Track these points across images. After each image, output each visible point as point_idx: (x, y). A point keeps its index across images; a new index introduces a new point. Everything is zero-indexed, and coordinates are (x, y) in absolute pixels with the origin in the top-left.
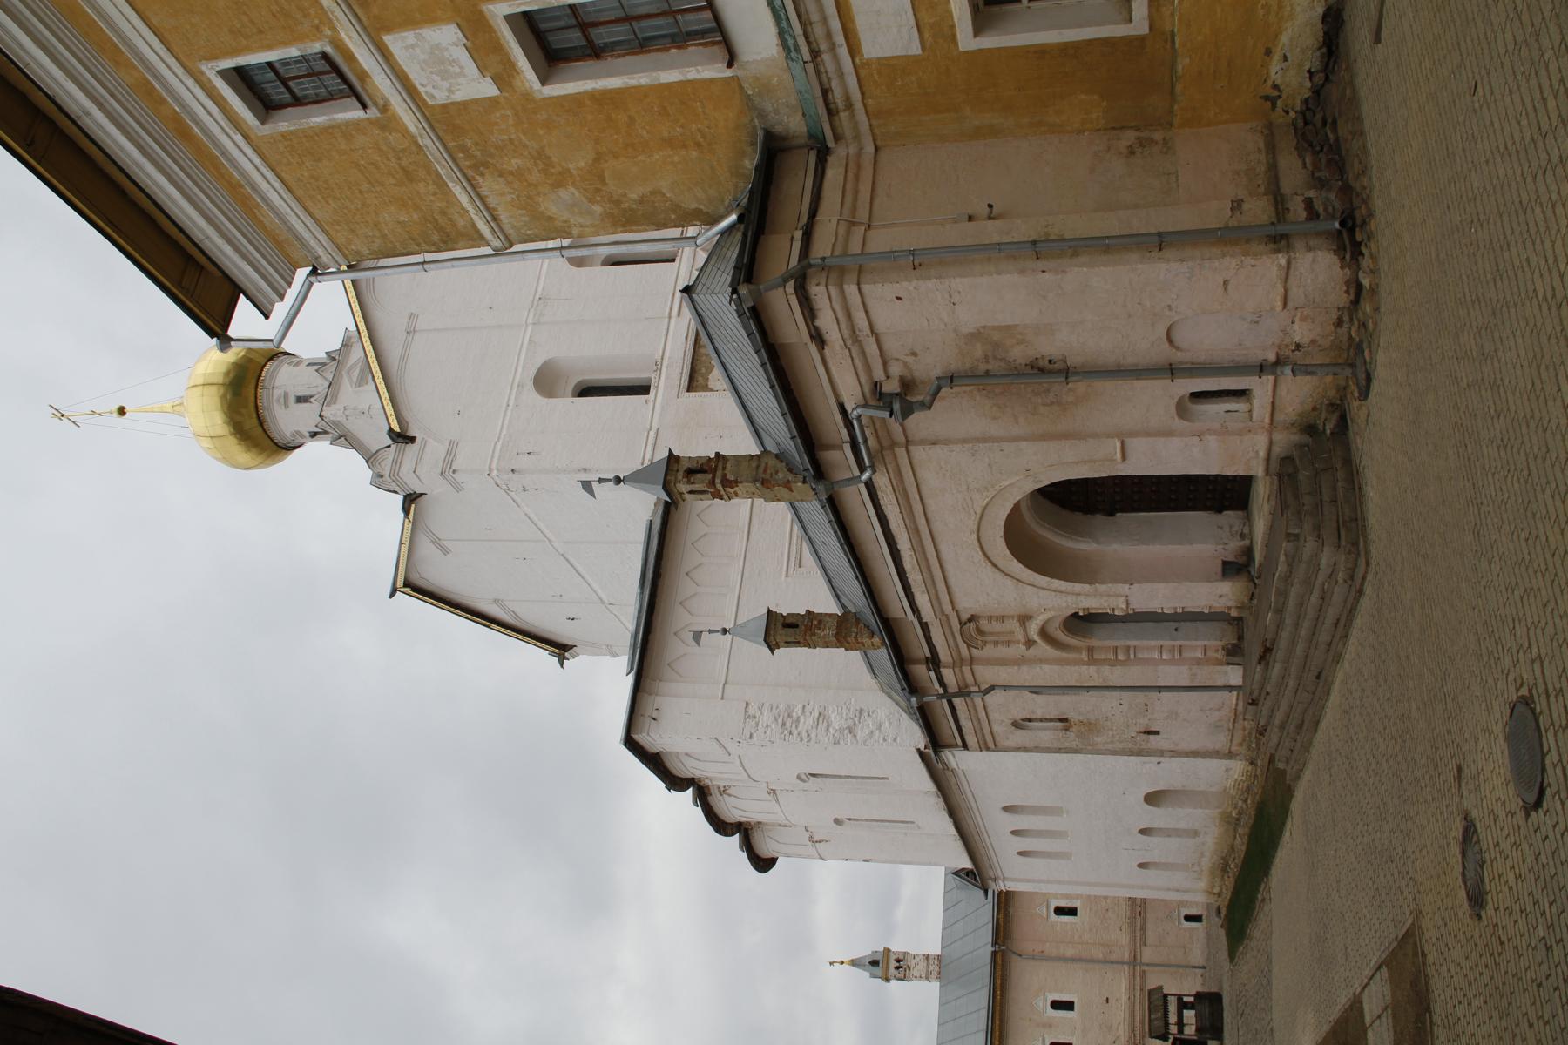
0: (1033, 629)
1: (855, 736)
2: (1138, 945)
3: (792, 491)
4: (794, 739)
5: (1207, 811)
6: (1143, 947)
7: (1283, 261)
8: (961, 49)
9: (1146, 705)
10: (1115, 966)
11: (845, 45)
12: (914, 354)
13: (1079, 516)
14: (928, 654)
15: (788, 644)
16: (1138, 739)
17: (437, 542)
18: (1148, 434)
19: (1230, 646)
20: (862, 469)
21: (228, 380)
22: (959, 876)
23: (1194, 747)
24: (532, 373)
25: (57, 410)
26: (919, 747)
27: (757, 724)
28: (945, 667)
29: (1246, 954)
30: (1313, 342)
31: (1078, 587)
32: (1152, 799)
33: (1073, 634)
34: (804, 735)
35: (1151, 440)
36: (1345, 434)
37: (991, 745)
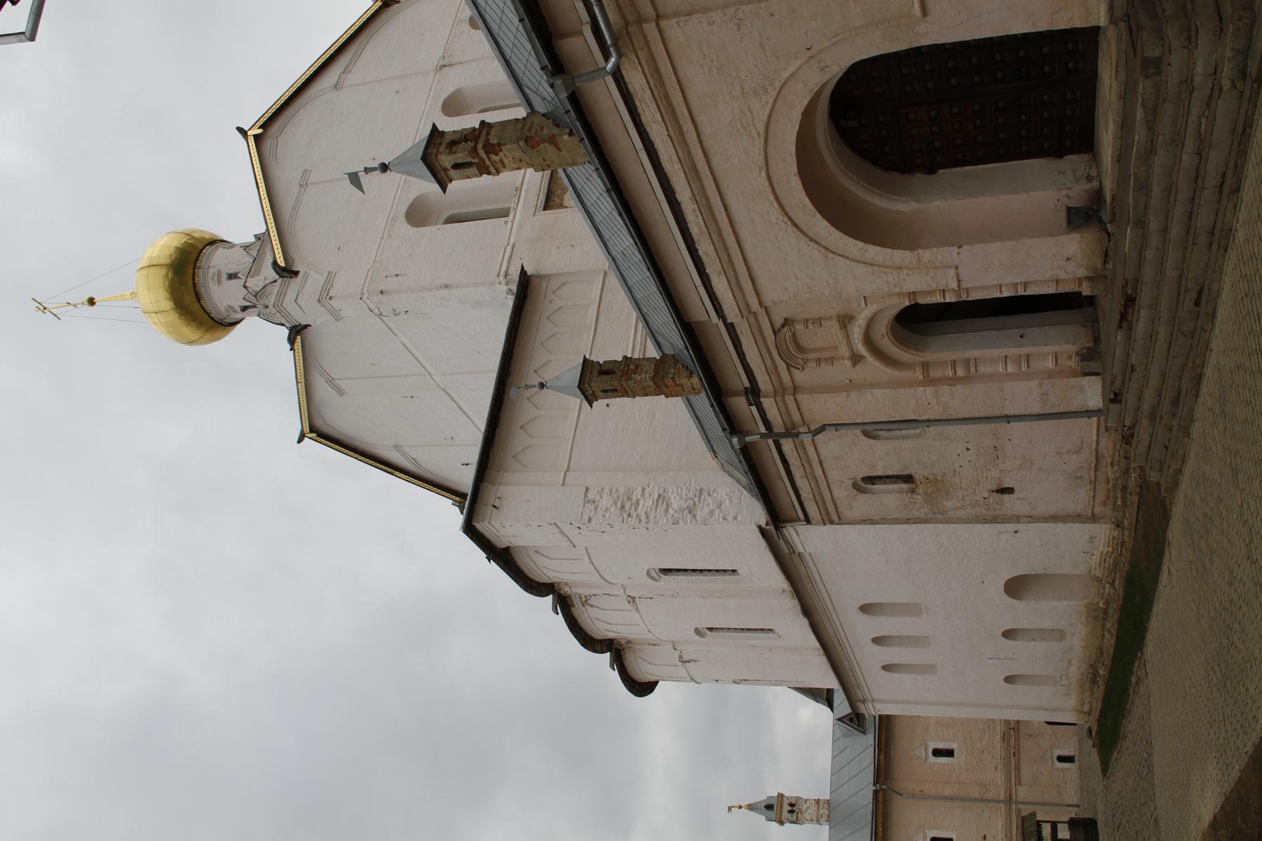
1: (695, 516)
2: (1013, 785)
3: (559, 149)
4: (633, 521)
6: (1018, 786)
10: (991, 804)
13: (895, 176)
14: (747, 384)
16: (991, 501)
17: (331, 381)
19: (1085, 351)
21: (168, 261)
23: (1053, 510)
24: (405, 207)
25: (40, 303)
26: (761, 524)
27: (596, 508)
28: (765, 397)
29: (1120, 758)
31: (898, 256)
32: (1016, 587)
34: (643, 517)
37: (836, 519)
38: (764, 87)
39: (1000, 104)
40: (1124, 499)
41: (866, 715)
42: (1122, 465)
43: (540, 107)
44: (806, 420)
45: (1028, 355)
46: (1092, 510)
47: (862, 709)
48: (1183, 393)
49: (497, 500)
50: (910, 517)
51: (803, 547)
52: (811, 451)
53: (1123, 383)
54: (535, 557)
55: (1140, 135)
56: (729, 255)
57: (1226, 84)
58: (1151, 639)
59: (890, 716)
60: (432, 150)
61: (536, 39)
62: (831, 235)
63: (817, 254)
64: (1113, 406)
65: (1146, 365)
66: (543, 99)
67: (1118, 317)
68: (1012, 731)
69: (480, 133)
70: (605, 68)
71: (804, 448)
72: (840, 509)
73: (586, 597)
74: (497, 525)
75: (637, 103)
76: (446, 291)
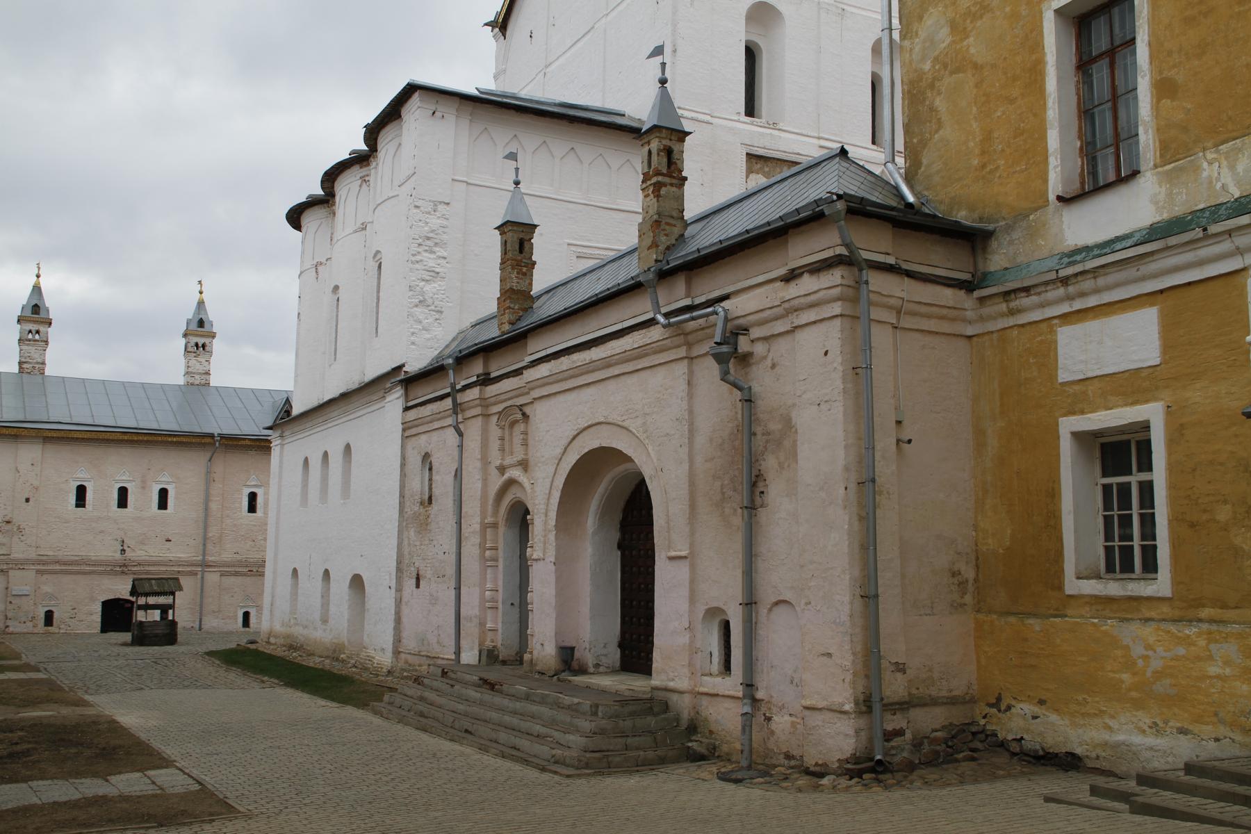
0: (515, 473)
1: (416, 306)
4: (414, 248)
5: (345, 631)
7: (847, 707)
8: (1060, 419)
9: (444, 576)
10: (201, 548)
11: (1071, 310)
12: (773, 366)
13: (618, 516)
14: (493, 375)
15: (505, 244)
16: (413, 569)
18: (692, 581)
20: (667, 315)
23: (404, 620)
27: (429, 213)
28: (481, 390)
30: (772, 733)
32: (357, 582)
34: (418, 258)
35: (687, 584)
44: (467, 421)
45: (497, 608)
49: (440, 114)
51: (389, 402)
54: (395, 143)
63: (559, 451)
67: (486, 678)
72: (414, 439)
73: (368, 181)
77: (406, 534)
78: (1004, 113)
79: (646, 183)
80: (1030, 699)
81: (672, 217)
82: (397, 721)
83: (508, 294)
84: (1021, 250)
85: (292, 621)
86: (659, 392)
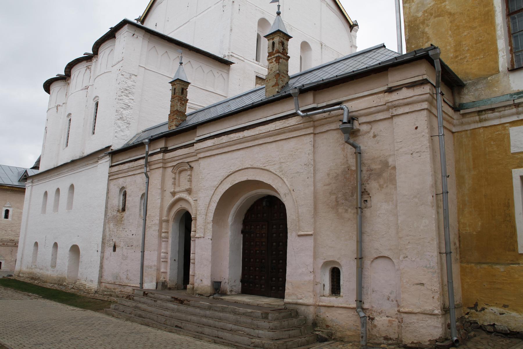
1: (119, 120)
3: (273, 86)
4: (120, 93)
5: (66, 272)
7: (436, 312)
8: (513, 170)
11: (518, 119)
12: (375, 136)
13: (243, 217)
14: (169, 148)
16: (111, 242)
18: (315, 247)
19: (166, 284)
20: (302, 111)
22: (25, 173)
23: (105, 267)
26: (112, 147)
27: (127, 78)
28: (163, 155)
30: (375, 326)
32: (75, 249)
33: (177, 213)
34: (121, 98)
35: (312, 249)
36: (317, 341)
38: (282, 171)
39: (264, 261)
40: (106, 295)
41: (26, 183)
42: (120, 295)
43: (291, 82)
46: (103, 282)
47: (29, 181)
48: (143, 319)
49: (136, 36)
50: (108, 209)
52: (139, 171)
53: (151, 297)
54: (110, 49)
55: (242, 310)
56: (220, 148)
57: (253, 340)
58: (47, 302)
59: (24, 195)
60: (281, 35)
61: (310, 86)
62: (223, 190)
63: (216, 183)
64: (142, 293)
65: (156, 306)
66: (294, 84)
67: (176, 297)
68: (15, 244)
69: (285, 56)
70: (299, 110)
71: (141, 168)
72: (114, 181)
73: (90, 68)
74: (125, 35)
75: (284, 121)
76: (229, 29)
77: (107, 226)
78: (468, 33)
79: (271, 56)
80: (497, 305)
81: (284, 73)
82: (125, 319)
83: (176, 112)
84: (483, 93)
85: (33, 266)
86: (292, 151)
